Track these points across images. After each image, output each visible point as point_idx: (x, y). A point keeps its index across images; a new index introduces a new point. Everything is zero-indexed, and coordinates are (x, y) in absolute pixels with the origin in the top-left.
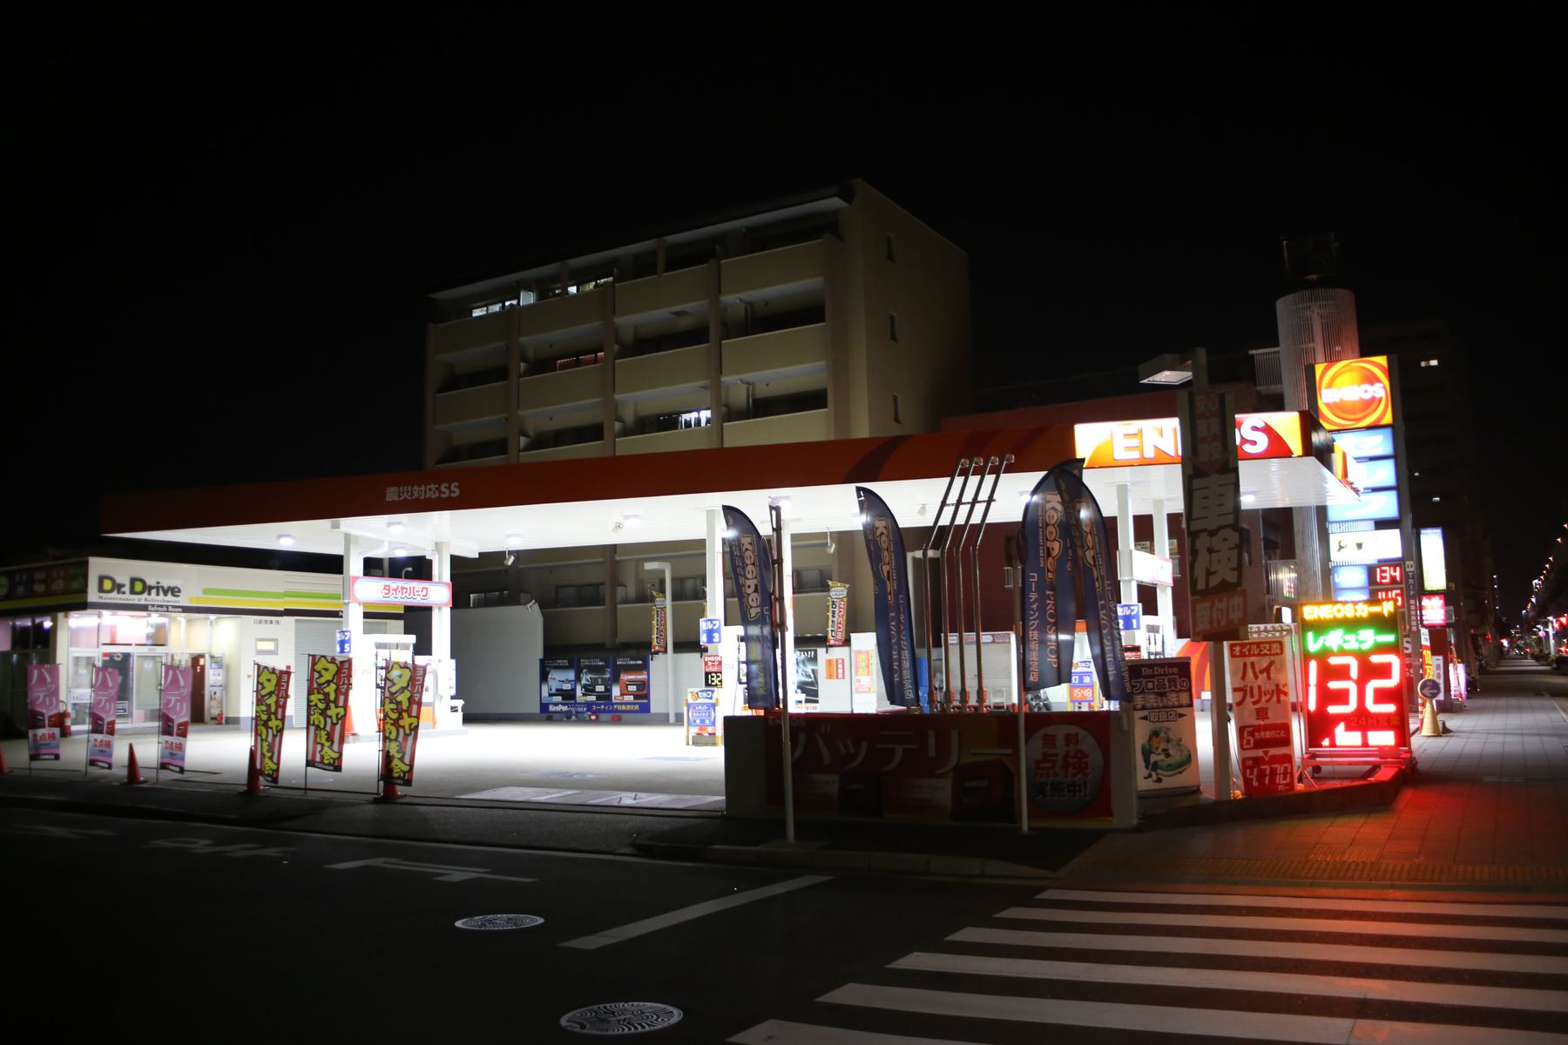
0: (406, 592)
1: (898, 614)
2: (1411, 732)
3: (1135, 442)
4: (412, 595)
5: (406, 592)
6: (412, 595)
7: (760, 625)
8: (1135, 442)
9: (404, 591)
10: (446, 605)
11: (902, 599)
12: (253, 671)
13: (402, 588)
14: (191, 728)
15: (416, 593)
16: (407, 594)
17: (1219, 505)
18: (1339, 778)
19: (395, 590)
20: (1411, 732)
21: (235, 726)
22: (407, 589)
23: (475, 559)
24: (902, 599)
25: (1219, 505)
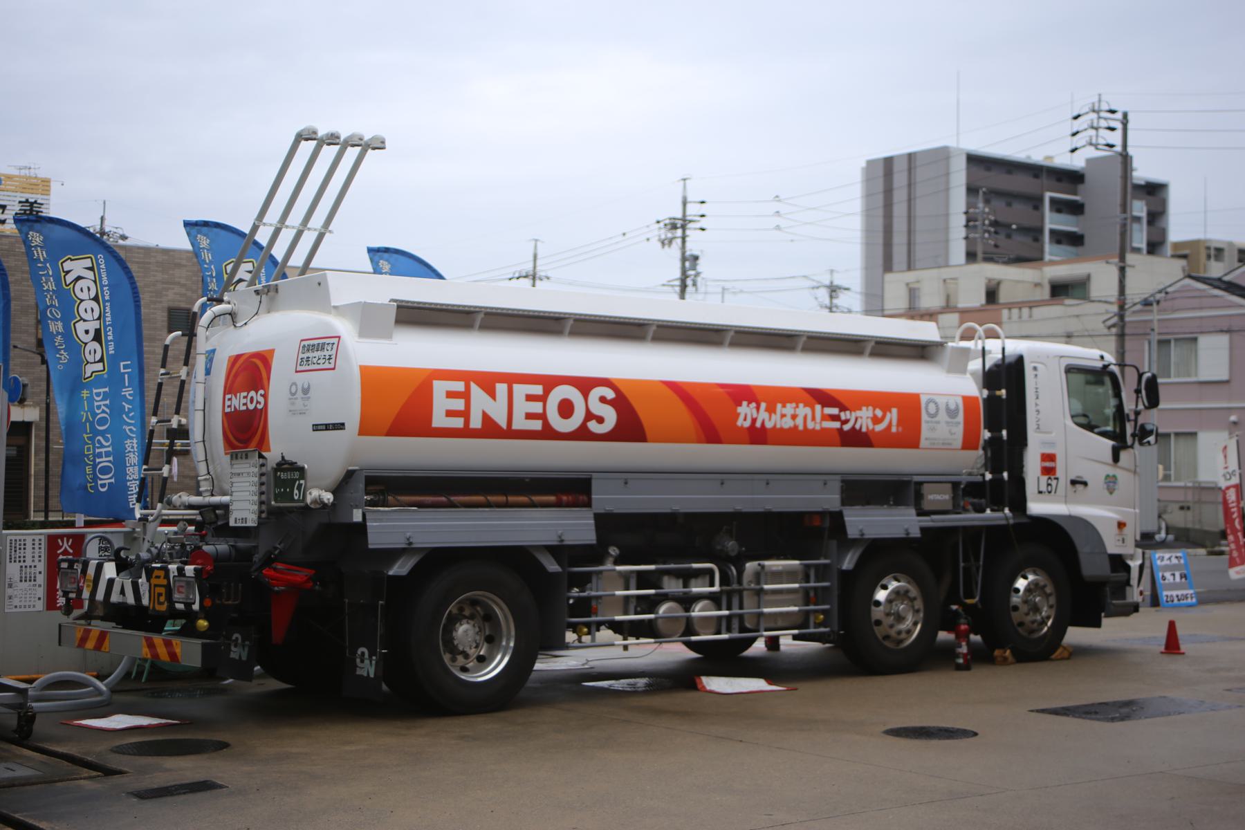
3: (459, 404)
8: (459, 404)
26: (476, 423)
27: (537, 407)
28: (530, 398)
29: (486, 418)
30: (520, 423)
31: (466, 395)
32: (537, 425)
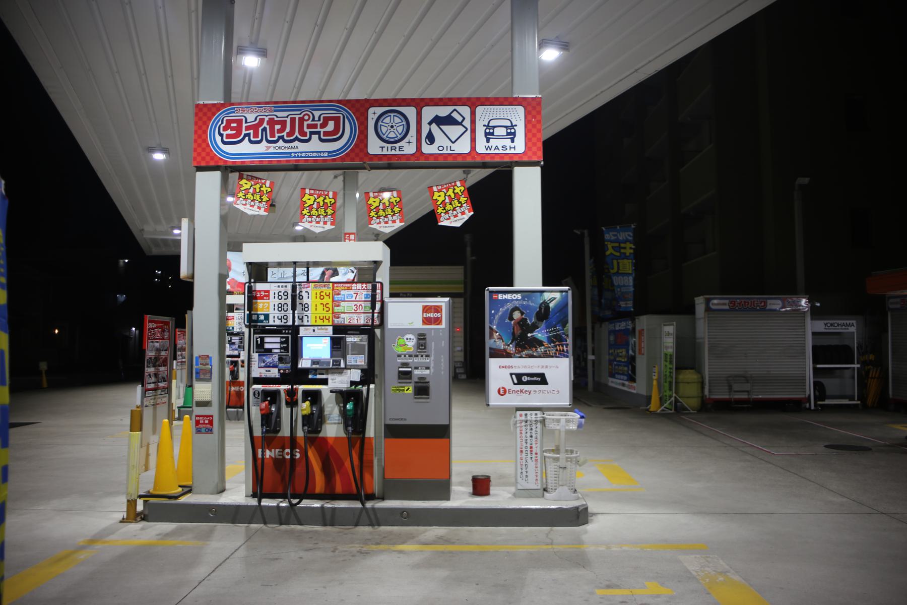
0: (748, 305)
1: (621, 365)
2: (441, 126)
4: (752, 306)
5: (281, 130)
6: (752, 306)
7: (366, 367)
9: (747, 304)
10: (698, 304)
11: (288, 454)
12: (638, 378)
13: (272, 122)
14: (259, 407)
15: (756, 305)
16: (749, 306)
17: (359, 596)
18: (320, 14)
19: (255, 128)
20: (441, 126)
21: (243, 421)
22: (748, 302)
23: (436, 124)
24: (288, 454)
25: (359, 596)
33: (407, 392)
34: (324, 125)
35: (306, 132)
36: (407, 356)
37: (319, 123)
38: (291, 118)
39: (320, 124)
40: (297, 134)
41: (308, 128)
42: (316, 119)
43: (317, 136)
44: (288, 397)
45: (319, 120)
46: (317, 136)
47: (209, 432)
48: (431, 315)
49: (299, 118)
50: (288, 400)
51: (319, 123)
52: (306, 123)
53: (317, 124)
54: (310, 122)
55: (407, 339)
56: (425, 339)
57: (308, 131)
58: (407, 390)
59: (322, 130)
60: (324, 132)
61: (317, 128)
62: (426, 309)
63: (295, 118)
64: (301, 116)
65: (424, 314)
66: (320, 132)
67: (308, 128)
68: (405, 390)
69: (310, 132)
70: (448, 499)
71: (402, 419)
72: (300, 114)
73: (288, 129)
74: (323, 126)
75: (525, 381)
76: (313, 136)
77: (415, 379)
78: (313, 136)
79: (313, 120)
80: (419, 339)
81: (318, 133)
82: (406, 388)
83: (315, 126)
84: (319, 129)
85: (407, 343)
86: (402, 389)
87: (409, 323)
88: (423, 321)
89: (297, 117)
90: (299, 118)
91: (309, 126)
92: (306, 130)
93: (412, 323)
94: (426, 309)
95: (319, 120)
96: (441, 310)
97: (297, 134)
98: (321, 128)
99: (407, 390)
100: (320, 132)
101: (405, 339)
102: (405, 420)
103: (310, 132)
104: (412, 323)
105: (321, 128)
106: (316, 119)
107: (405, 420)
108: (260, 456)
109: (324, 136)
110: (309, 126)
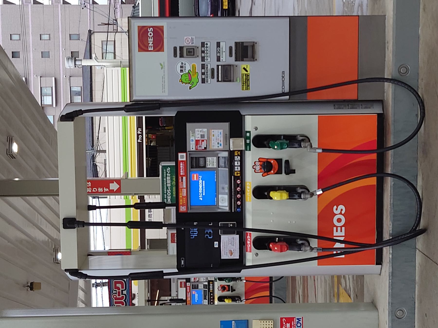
3: (151, 47)
8: (151, 47)
26: (152, 45)
27: (151, 38)
28: (150, 39)
29: (152, 44)
30: (152, 40)
31: (150, 46)
32: (152, 38)
33: (248, 71)
34: (119, 289)
35: (122, 296)
36: (203, 71)
37: (117, 291)
38: (115, 303)
39: (118, 290)
40: (122, 301)
41: (120, 296)
42: (115, 292)
43: (124, 291)
44: (272, 172)
45: (116, 291)
46: (124, 291)
47: (301, 322)
48: (151, 41)
49: (115, 300)
50: (275, 171)
51: (117, 291)
52: (117, 297)
53: (118, 292)
54: (117, 295)
55: (181, 71)
56: (181, 48)
57: (121, 296)
58: (247, 71)
59: (121, 289)
60: (122, 288)
61: (120, 292)
62: (143, 47)
63: (115, 302)
64: (114, 299)
65: (149, 49)
66: (122, 290)
67: (120, 296)
68: (246, 73)
69: (122, 294)
70: (384, 17)
71: (283, 77)
72: (113, 299)
73: (121, 305)
74: (119, 289)
75: (237, 182)
76: (124, 293)
77: (231, 61)
78: (124, 293)
79: (116, 293)
80: (181, 56)
81: (122, 291)
82: (245, 72)
83: (119, 292)
84: (121, 291)
85: (187, 72)
86: (244, 77)
87: (162, 69)
88: (158, 51)
89: (114, 301)
90: (115, 300)
91: (119, 295)
92: (120, 297)
93: (161, 64)
94: (143, 47)
95: (116, 291)
96: (180, 157)
97: (122, 301)
98: (120, 290)
99: (247, 71)
100: (122, 290)
101: (182, 74)
102: (283, 72)
103: (122, 294)
104: (161, 64)
105: (120, 290)
106: (115, 292)
107: (283, 72)
108: (343, 246)
109: (123, 288)
110: (119, 295)
